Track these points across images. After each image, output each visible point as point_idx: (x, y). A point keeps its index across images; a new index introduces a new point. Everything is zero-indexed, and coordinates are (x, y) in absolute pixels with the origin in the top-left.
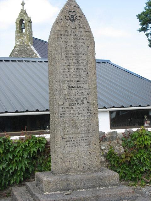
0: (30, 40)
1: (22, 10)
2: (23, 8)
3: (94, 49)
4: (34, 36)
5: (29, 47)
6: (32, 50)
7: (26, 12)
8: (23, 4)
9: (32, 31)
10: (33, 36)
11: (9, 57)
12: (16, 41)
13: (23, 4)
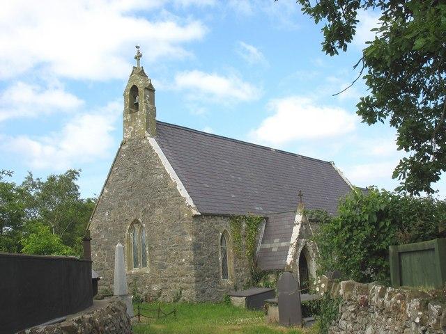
0: (147, 127)
1: (134, 67)
2: (138, 64)
3: (303, 157)
4: (160, 117)
5: (145, 141)
6: (151, 147)
7: (143, 71)
8: (138, 57)
9: (155, 108)
10: (158, 118)
11: (159, 123)
12: (124, 131)
13: (138, 57)
